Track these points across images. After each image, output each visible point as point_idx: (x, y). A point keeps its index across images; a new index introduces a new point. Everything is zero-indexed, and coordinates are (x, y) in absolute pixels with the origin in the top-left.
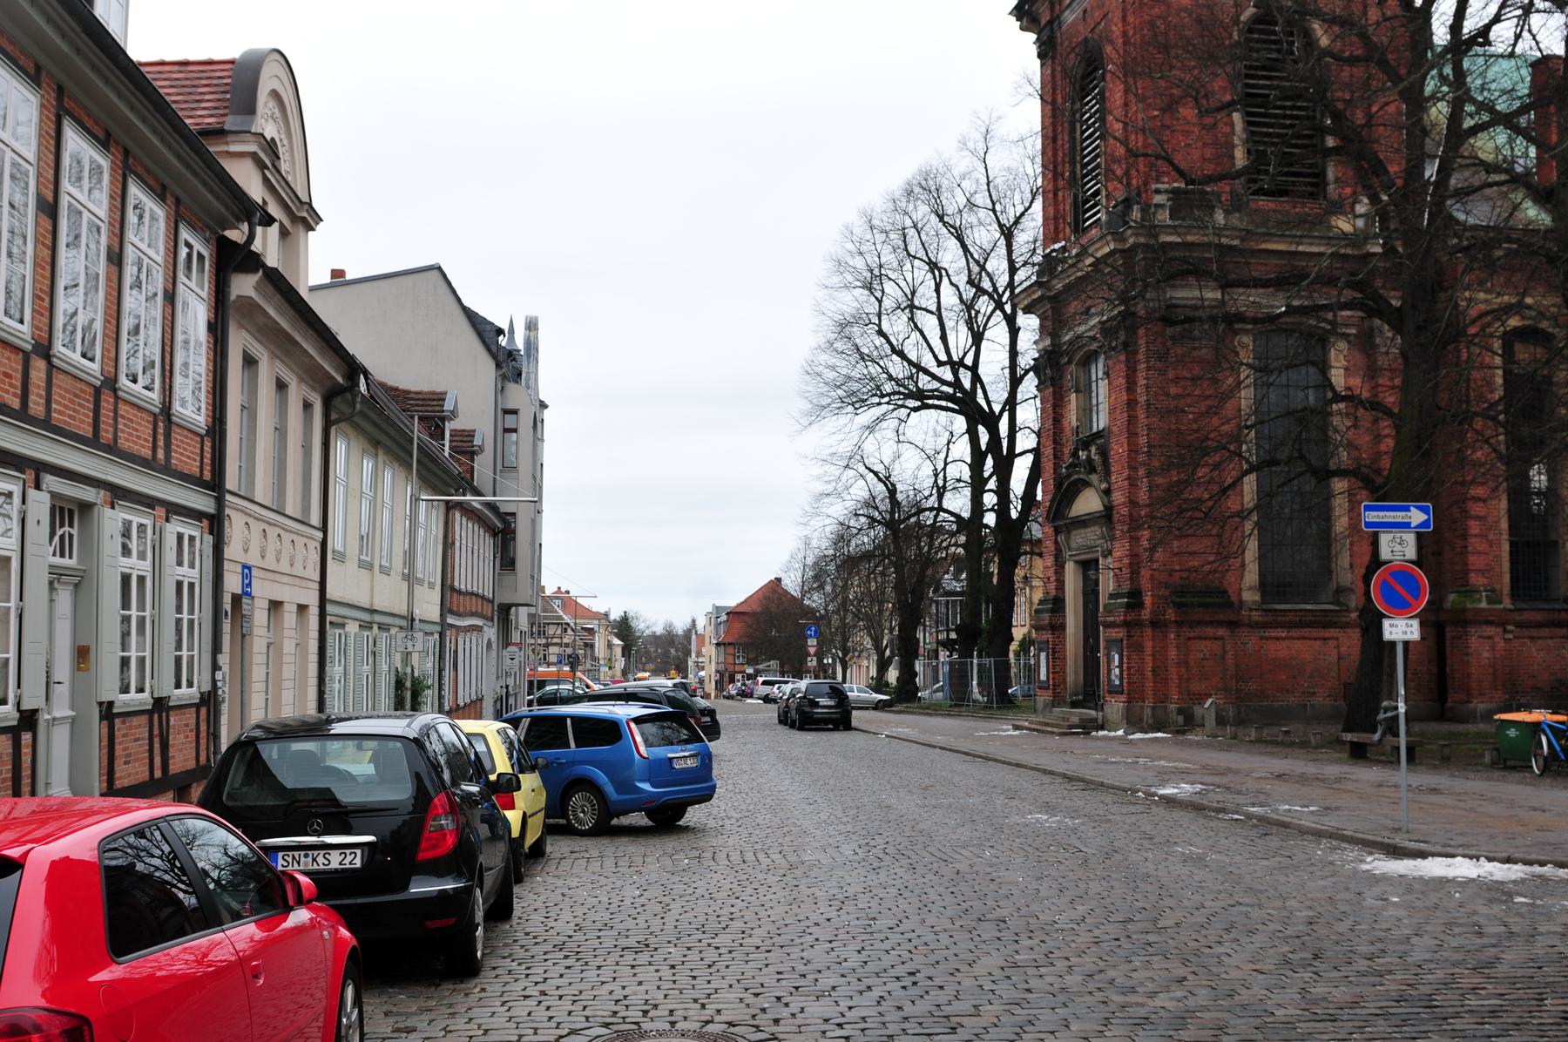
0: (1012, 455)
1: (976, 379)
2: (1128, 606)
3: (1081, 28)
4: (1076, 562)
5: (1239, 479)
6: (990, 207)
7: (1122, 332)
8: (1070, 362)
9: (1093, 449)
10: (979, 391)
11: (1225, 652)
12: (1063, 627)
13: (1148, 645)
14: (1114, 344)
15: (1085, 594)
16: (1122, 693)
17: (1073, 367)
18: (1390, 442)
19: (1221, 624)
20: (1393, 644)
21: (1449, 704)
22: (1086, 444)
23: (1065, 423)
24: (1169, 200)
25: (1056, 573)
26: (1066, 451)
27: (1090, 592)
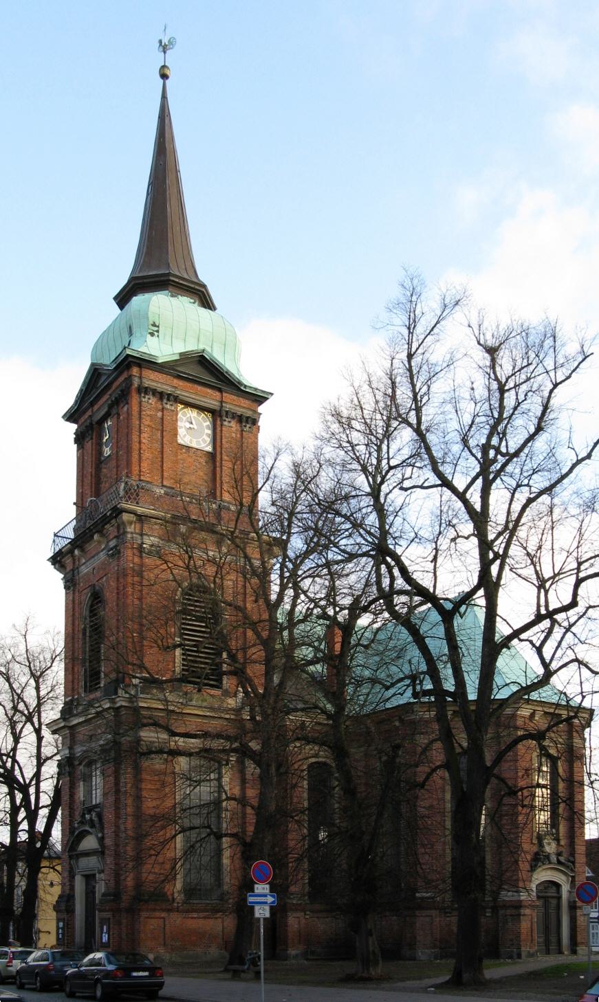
0: (37, 808)
1: (14, 761)
3: (91, 577)
5: (175, 836)
6: (28, 665)
7: (113, 752)
8: (80, 764)
9: (94, 814)
10: (17, 767)
11: (165, 925)
15: (87, 893)
17: (81, 767)
18: (375, 579)
19: (163, 910)
20: (259, 919)
23: (76, 797)
25: (70, 881)
27: (90, 893)
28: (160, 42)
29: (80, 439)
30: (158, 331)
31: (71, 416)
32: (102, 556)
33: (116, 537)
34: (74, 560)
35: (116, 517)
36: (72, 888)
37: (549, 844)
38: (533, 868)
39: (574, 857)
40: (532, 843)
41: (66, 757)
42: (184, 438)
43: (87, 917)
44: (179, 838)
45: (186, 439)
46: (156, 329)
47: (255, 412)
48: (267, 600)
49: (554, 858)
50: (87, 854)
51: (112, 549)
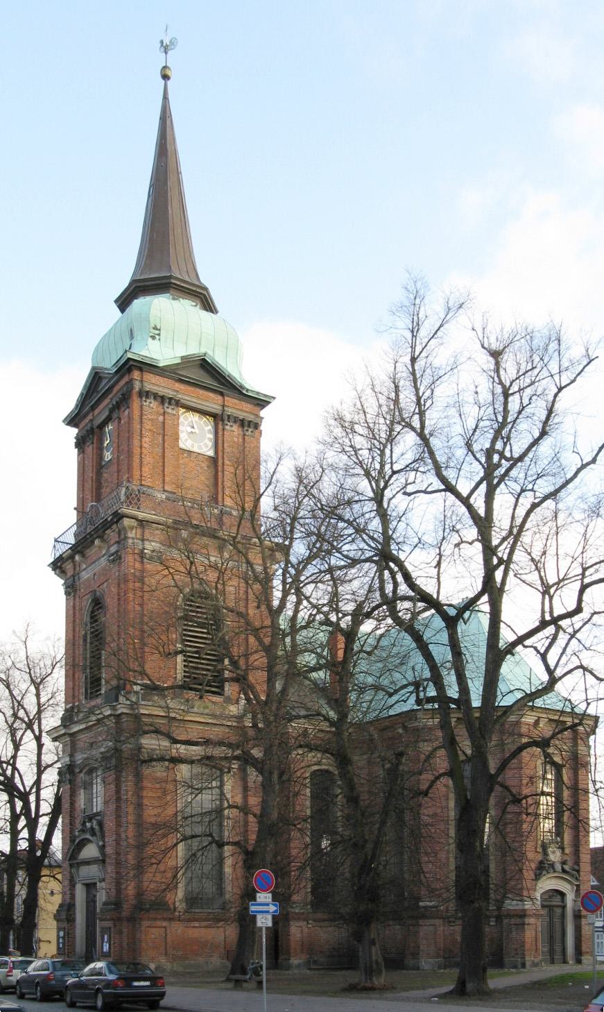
0: (38, 816)
1: (15, 768)
2: (114, 909)
4: (84, 884)
5: (176, 845)
6: (28, 671)
8: (81, 772)
9: (95, 822)
10: (17, 775)
12: (74, 920)
13: (125, 930)
14: (108, 766)
16: (110, 956)
17: (82, 775)
19: (165, 919)
21: (280, 961)
22: (90, 818)
24: (141, 689)
25: (70, 890)
26: (78, 822)
27: (91, 901)
28: (162, 42)
29: (80, 443)
30: (159, 335)
31: (72, 420)
32: (103, 562)
33: (118, 542)
34: (75, 566)
35: (117, 522)
36: (73, 896)
37: (554, 852)
38: (537, 877)
39: (579, 865)
40: (537, 852)
41: (66, 765)
42: (185, 442)
43: (88, 926)
44: (181, 847)
45: (187, 444)
46: (157, 332)
47: (257, 416)
48: (269, 607)
49: (558, 867)
50: (87, 863)
51: (113, 555)
